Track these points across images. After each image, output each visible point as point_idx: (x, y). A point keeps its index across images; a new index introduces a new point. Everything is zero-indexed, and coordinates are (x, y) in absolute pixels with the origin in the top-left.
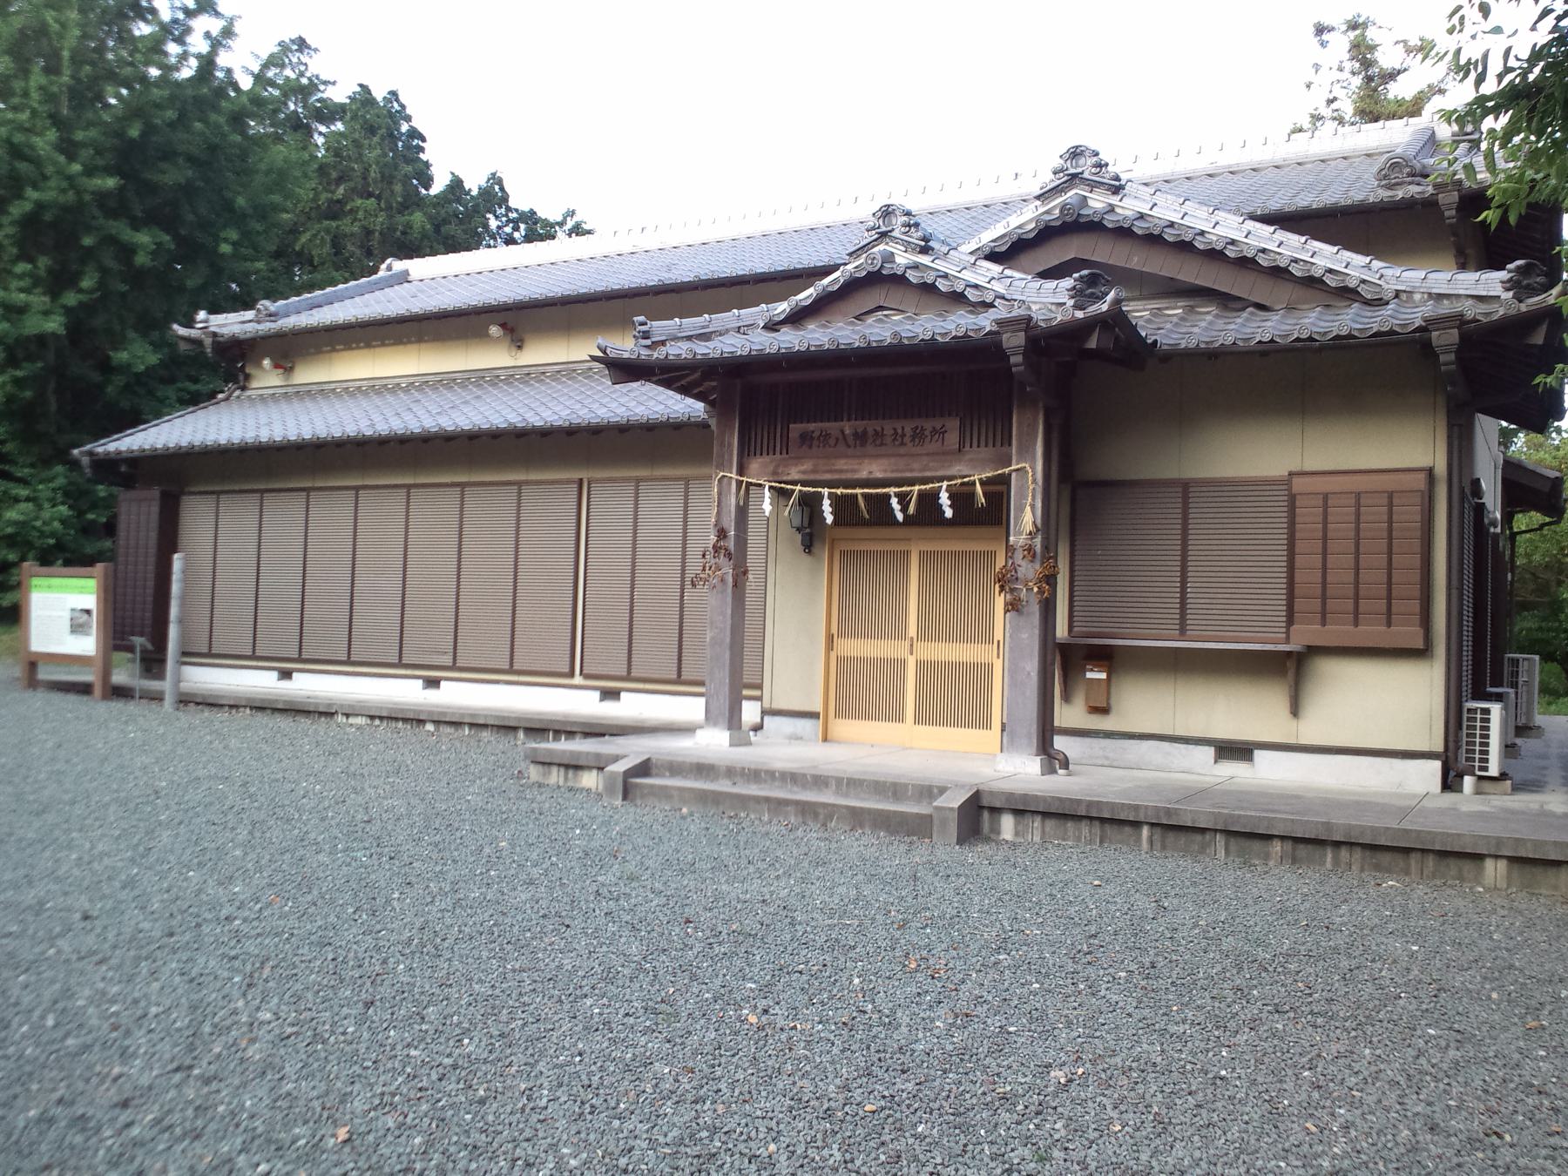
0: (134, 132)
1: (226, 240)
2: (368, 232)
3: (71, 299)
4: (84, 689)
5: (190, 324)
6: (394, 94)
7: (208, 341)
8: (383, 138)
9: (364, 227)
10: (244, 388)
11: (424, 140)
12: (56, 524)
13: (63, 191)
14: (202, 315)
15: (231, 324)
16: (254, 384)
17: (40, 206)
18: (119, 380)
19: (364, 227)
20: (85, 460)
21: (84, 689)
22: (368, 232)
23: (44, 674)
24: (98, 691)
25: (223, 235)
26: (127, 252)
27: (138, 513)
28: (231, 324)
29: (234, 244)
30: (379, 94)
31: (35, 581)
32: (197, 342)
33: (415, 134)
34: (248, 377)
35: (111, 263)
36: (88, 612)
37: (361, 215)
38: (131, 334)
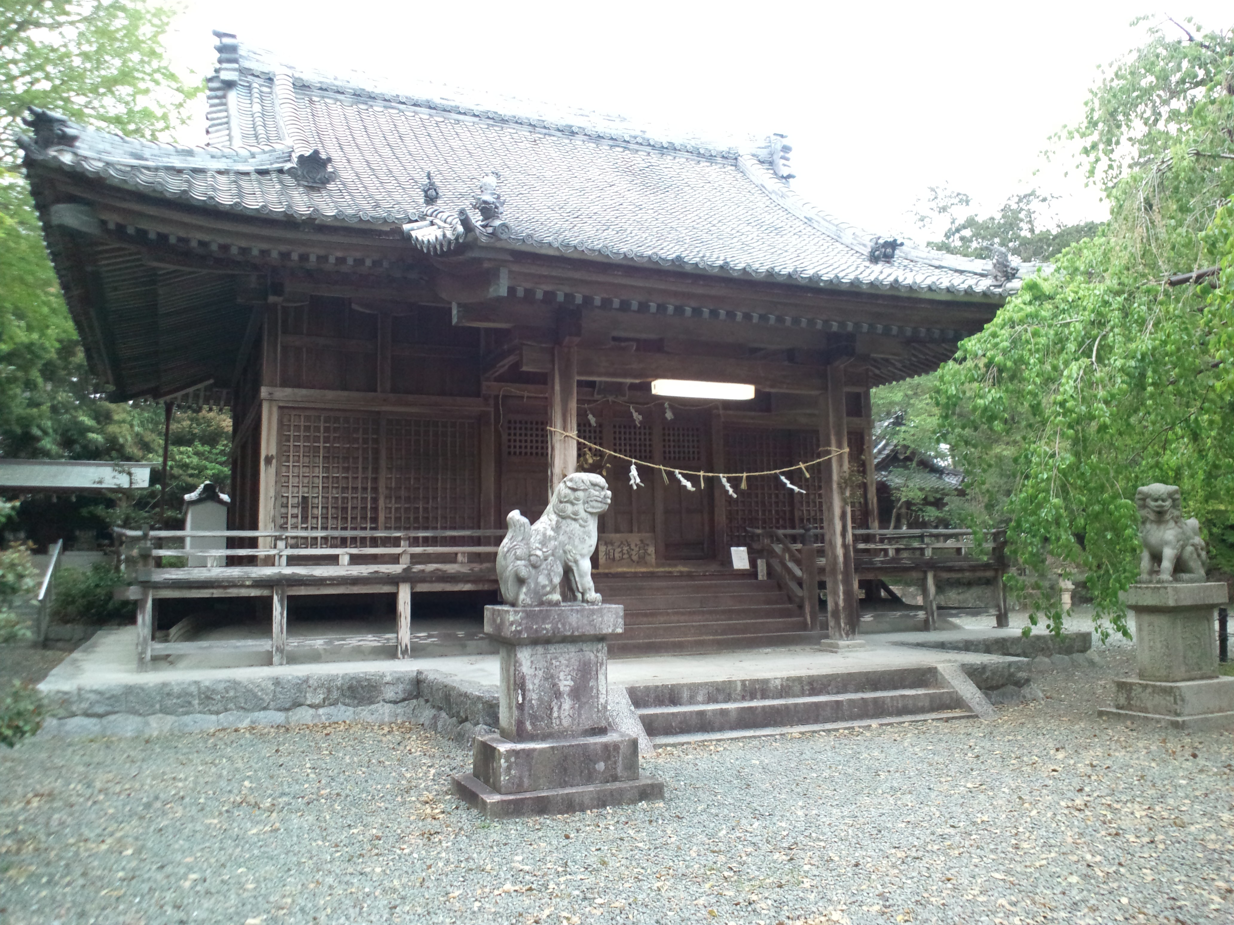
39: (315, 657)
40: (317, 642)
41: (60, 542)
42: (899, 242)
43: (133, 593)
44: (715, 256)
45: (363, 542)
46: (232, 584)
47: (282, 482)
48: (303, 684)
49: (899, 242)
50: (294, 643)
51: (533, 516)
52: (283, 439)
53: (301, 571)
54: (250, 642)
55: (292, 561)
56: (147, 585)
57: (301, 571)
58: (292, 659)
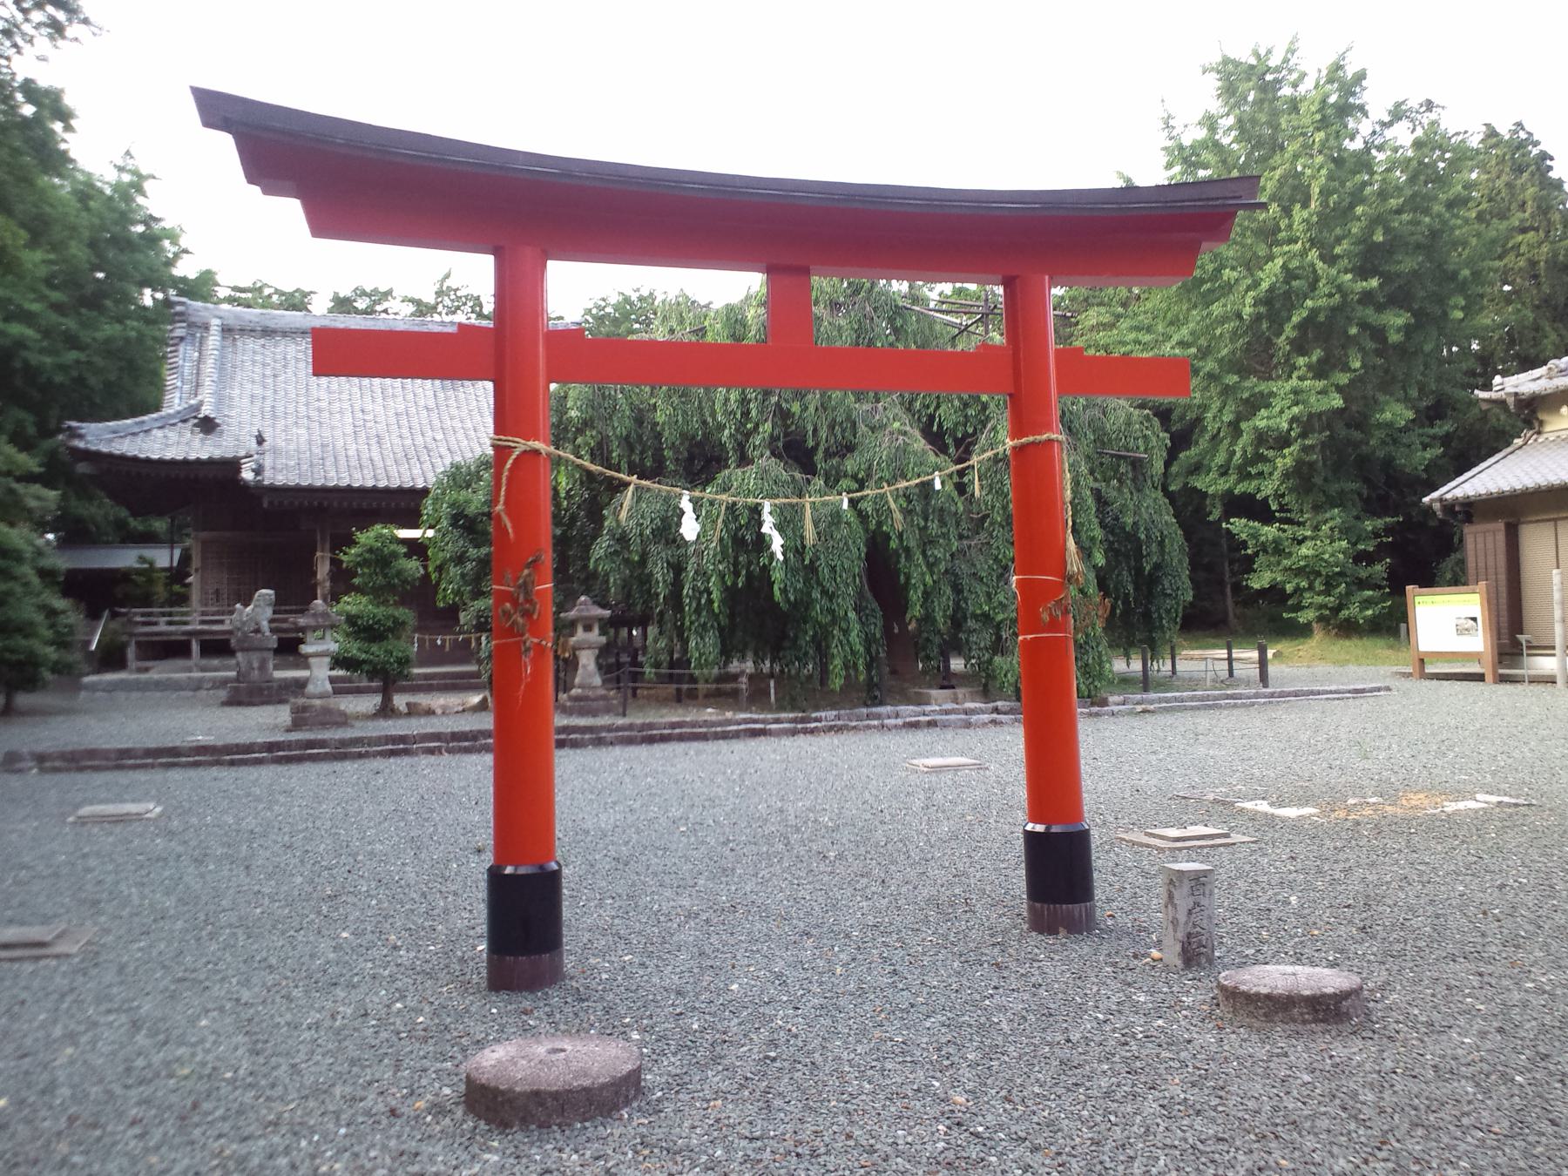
0: (1379, 237)
1: (1456, 307)
2: (1533, 263)
3: (1343, 379)
4: (1479, 678)
5: (1487, 387)
6: (1519, 125)
7: (1511, 401)
8: (1532, 174)
9: (1529, 260)
10: (1539, 433)
11: (1552, 159)
12: (1341, 556)
13: (1330, 295)
14: (1497, 379)
15: (1526, 383)
16: (1548, 428)
17: (1314, 312)
18: (1380, 434)
19: (1529, 260)
20: (1437, 506)
21: (1479, 678)
22: (1533, 263)
23: (1429, 669)
24: (1489, 677)
25: (1451, 303)
26: (1378, 334)
27: (1482, 542)
28: (1526, 383)
29: (1462, 309)
30: (1504, 130)
31: (1418, 599)
32: (1501, 403)
33: (1545, 156)
34: (1541, 423)
35: (1370, 345)
36: (1474, 619)
37: (1523, 249)
38: (1382, 398)
39: (216, 669)
40: (216, 662)
41: (106, 613)
42: (73, 122)
43: (124, 638)
44: (452, 402)
45: (170, 614)
46: (171, 633)
47: (203, 581)
48: (201, 680)
49: (73, 122)
50: (204, 662)
51: (246, 605)
52: (204, 559)
53: (205, 627)
54: (1506, 487)
55: (203, 622)
56: (132, 635)
57: (205, 627)
58: (203, 670)
